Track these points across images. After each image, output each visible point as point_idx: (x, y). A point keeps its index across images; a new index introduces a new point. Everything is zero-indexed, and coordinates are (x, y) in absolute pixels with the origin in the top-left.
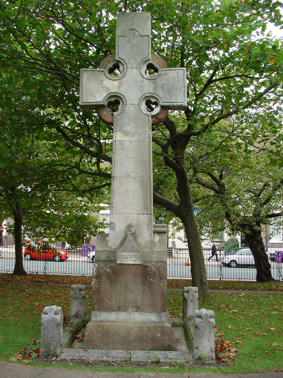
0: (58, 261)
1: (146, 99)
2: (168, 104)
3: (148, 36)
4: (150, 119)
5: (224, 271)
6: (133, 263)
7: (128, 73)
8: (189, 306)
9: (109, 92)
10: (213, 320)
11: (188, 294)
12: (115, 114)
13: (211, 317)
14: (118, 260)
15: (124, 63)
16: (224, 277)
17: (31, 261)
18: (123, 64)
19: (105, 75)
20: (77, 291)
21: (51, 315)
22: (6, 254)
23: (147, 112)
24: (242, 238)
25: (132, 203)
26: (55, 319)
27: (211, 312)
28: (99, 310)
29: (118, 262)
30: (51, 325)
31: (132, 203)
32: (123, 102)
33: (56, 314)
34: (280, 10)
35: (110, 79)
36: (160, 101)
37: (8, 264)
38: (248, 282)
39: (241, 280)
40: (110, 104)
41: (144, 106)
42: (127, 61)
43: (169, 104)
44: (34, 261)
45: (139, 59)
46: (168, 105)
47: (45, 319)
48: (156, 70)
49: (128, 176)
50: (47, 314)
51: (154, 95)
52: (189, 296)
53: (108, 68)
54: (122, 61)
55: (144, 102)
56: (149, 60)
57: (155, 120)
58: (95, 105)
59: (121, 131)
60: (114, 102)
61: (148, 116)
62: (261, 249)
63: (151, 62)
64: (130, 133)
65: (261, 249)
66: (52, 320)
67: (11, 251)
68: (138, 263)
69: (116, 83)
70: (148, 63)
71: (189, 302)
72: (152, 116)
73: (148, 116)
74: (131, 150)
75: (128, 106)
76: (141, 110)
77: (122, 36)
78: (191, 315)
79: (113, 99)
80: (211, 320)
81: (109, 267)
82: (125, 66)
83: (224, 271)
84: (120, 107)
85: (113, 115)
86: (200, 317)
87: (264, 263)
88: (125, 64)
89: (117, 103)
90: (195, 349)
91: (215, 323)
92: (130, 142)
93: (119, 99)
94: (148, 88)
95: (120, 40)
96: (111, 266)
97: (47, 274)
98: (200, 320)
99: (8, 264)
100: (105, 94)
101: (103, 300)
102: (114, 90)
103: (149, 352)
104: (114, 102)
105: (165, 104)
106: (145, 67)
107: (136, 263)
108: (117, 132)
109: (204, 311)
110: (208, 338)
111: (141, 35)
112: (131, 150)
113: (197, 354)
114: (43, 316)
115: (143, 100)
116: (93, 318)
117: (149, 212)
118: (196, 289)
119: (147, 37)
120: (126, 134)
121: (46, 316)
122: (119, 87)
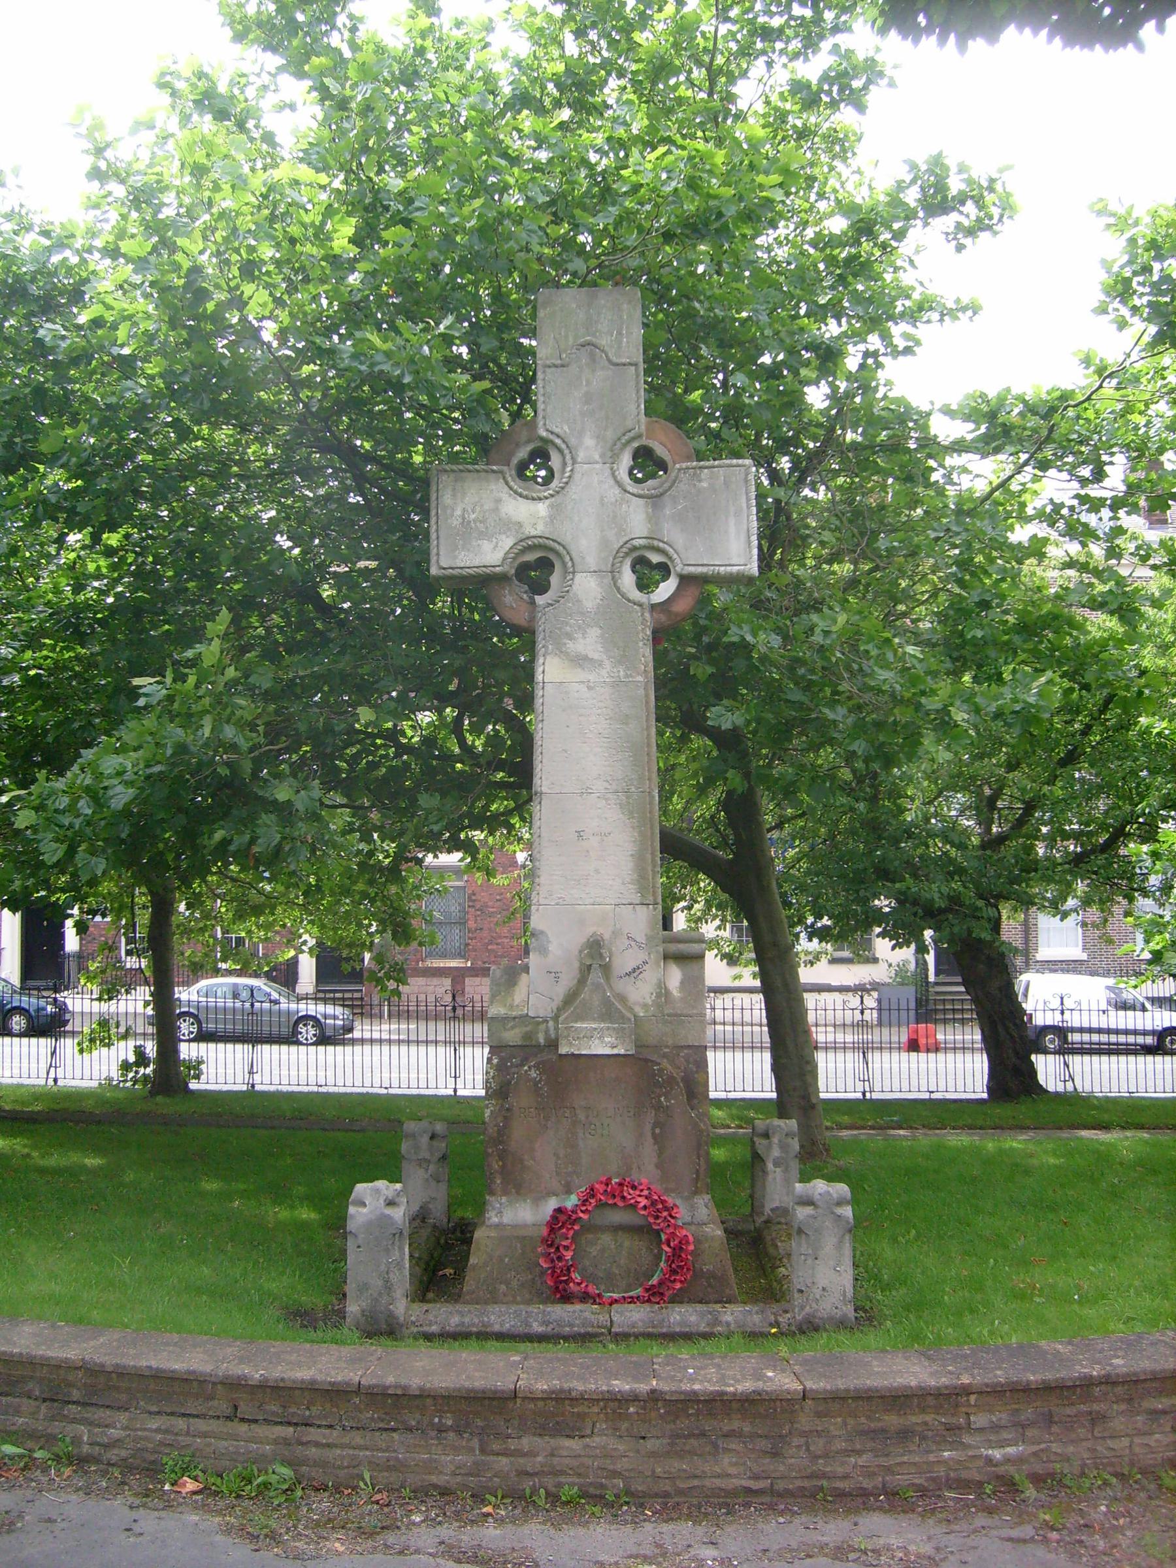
0: (189, 1041)
1: (635, 555)
2: (700, 570)
3: (636, 365)
4: (647, 615)
5: (877, 1066)
6: (608, 1051)
7: (577, 476)
8: (770, 1177)
9: (521, 536)
10: (847, 1212)
11: (764, 1142)
12: (540, 600)
14: (562, 1042)
15: (563, 446)
16: (877, 1087)
17: (321, 1048)
19: (507, 483)
20: (425, 1139)
22: (87, 1019)
23: (636, 595)
25: (597, 871)
26: (389, 1217)
27: (841, 1189)
28: (505, 1193)
29: (563, 1050)
31: (597, 871)
32: (564, 564)
33: (391, 1203)
34: (893, 948)
35: (521, 495)
36: (678, 561)
37: (395, 1062)
38: (961, 1101)
39: (934, 1096)
40: (523, 571)
41: (628, 579)
42: (573, 441)
43: (704, 570)
44: (330, 1048)
45: (610, 434)
47: (360, 1220)
48: (662, 465)
49: (586, 792)
50: (364, 1205)
51: (656, 543)
52: (769, 1147)
54: (558, 441)
56: (640, 436)
57: (663, 618)
58: (480, 575)
59: (561, 652)
60: (538, 567)
61: (641, 605)
62: (1000, 989)
63: (644, 441)
64: (586, 658)
65: (1000, 989)
66: (383, 1221)
67: (131, 1010)
68: (622, 1052)
69: (542, 508)
70: (636, 444)
71: (770, 1166)
72: (653, 607)
73: (641, 605)
74: (588, 712)
75: (578, 576)
76: (618, 589)
77: (556, 366)
78: (777, 1204)
79: (531, 557)
80: (839, 1211)
81: (537, 1066)
82: (568, 457)
83: (877, 1066)
84: (555, 579)
85: (533, 603)
86: (808, 1202)
87: (1012, 1037)
88: (566, 452)
89: (545, 565)
90: (796, 1295)
92: (589, 688)
93: (552, 557)
94: (637, 522)
95: (549, 377)
96: (543, 1062)
97: (257, 1088)
98: (809, 1210)
99: (395, 1062)
100: (507, 542)
101: (521, 1161)
102: (538, 529)
104: (538, 567)
105: (692, 569)
106: (626, 460)
107: (615, 1051)
108: (548, 658)
109: (820, 1186)
110: (832, 1263)
111: (615, 360)
112: (588, 712)
113: (802, 1308)
114: (352, 1210)
116: (493, 1218)
118: (792, 1124)
120: (580, 661)
122: (552, 518)
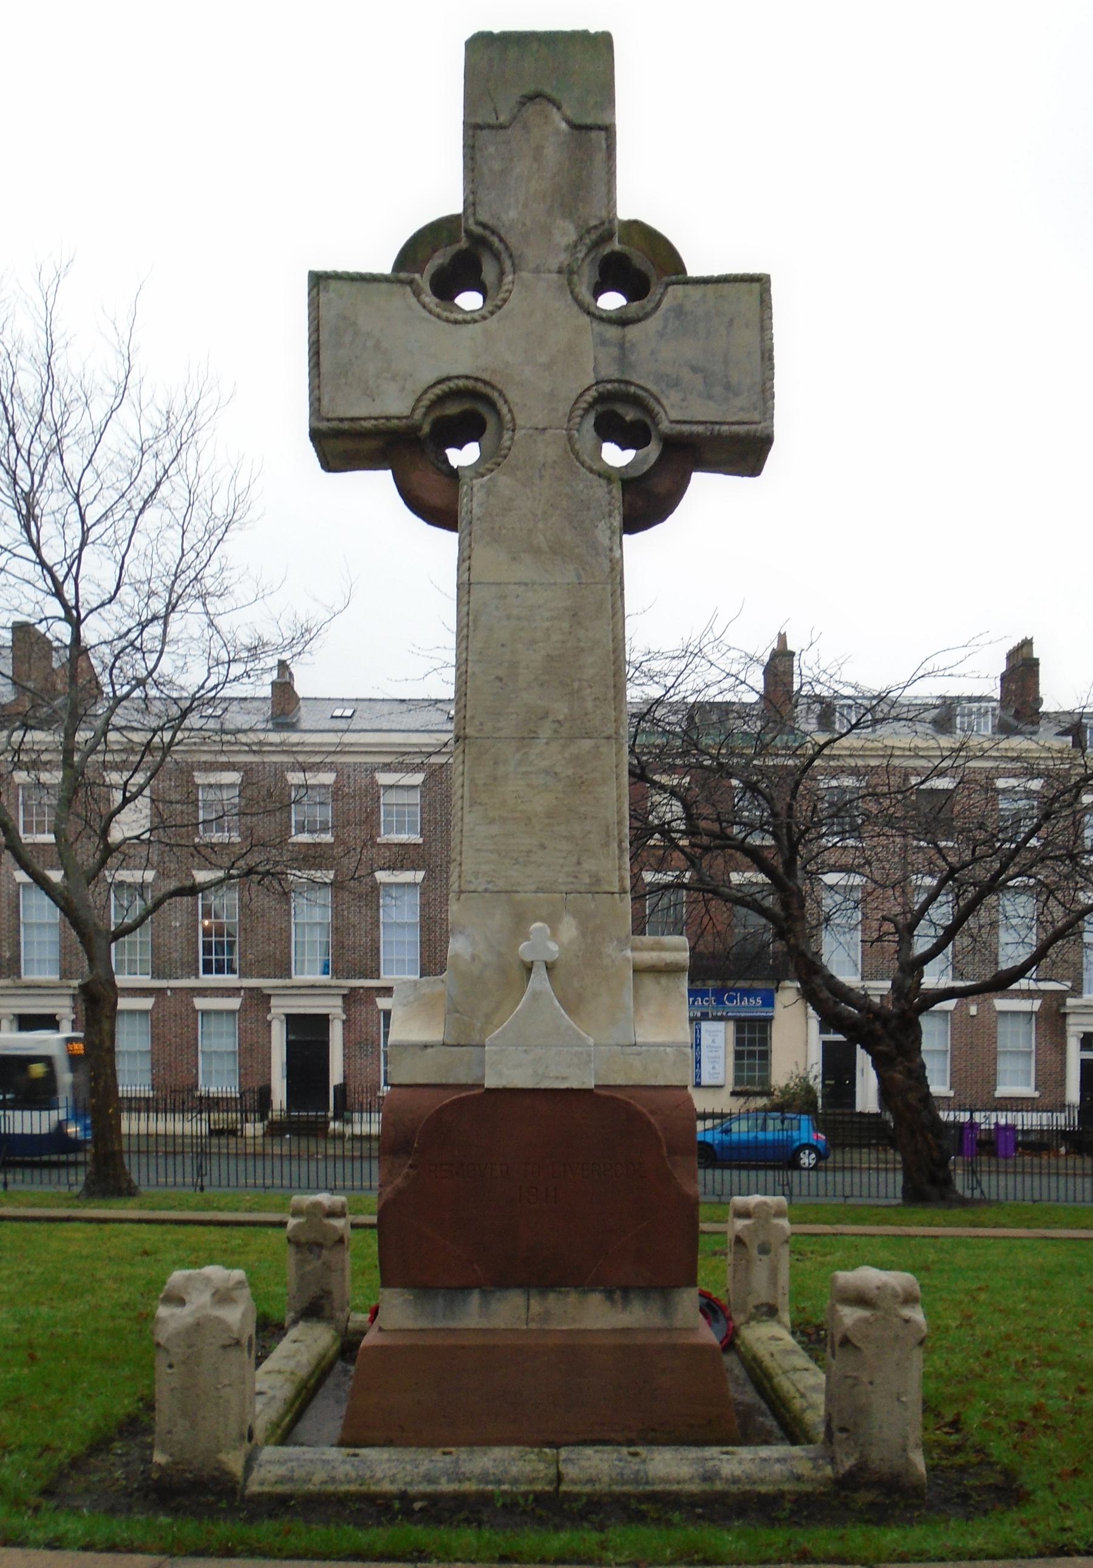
1: (599, 408)
13: (909, 1299)
18: (497, 256)
21: (199, 1301)
24: (827, 1082)
26: (220, 1321)
30: (170, 1044)
46: (691, 434)
47: (172, 1326)
50: (181, 1302)
53: (430, 268)
55: (591, 420)
75: (519, 434)
79: (453, 409)
91: (925, 1328)
93: (482, 409)
98: (860, 1313)
103: (450, 1453)
115: (582, 417)
117: (617, 884)
119: (603, 134)
121: (177, 1311)
